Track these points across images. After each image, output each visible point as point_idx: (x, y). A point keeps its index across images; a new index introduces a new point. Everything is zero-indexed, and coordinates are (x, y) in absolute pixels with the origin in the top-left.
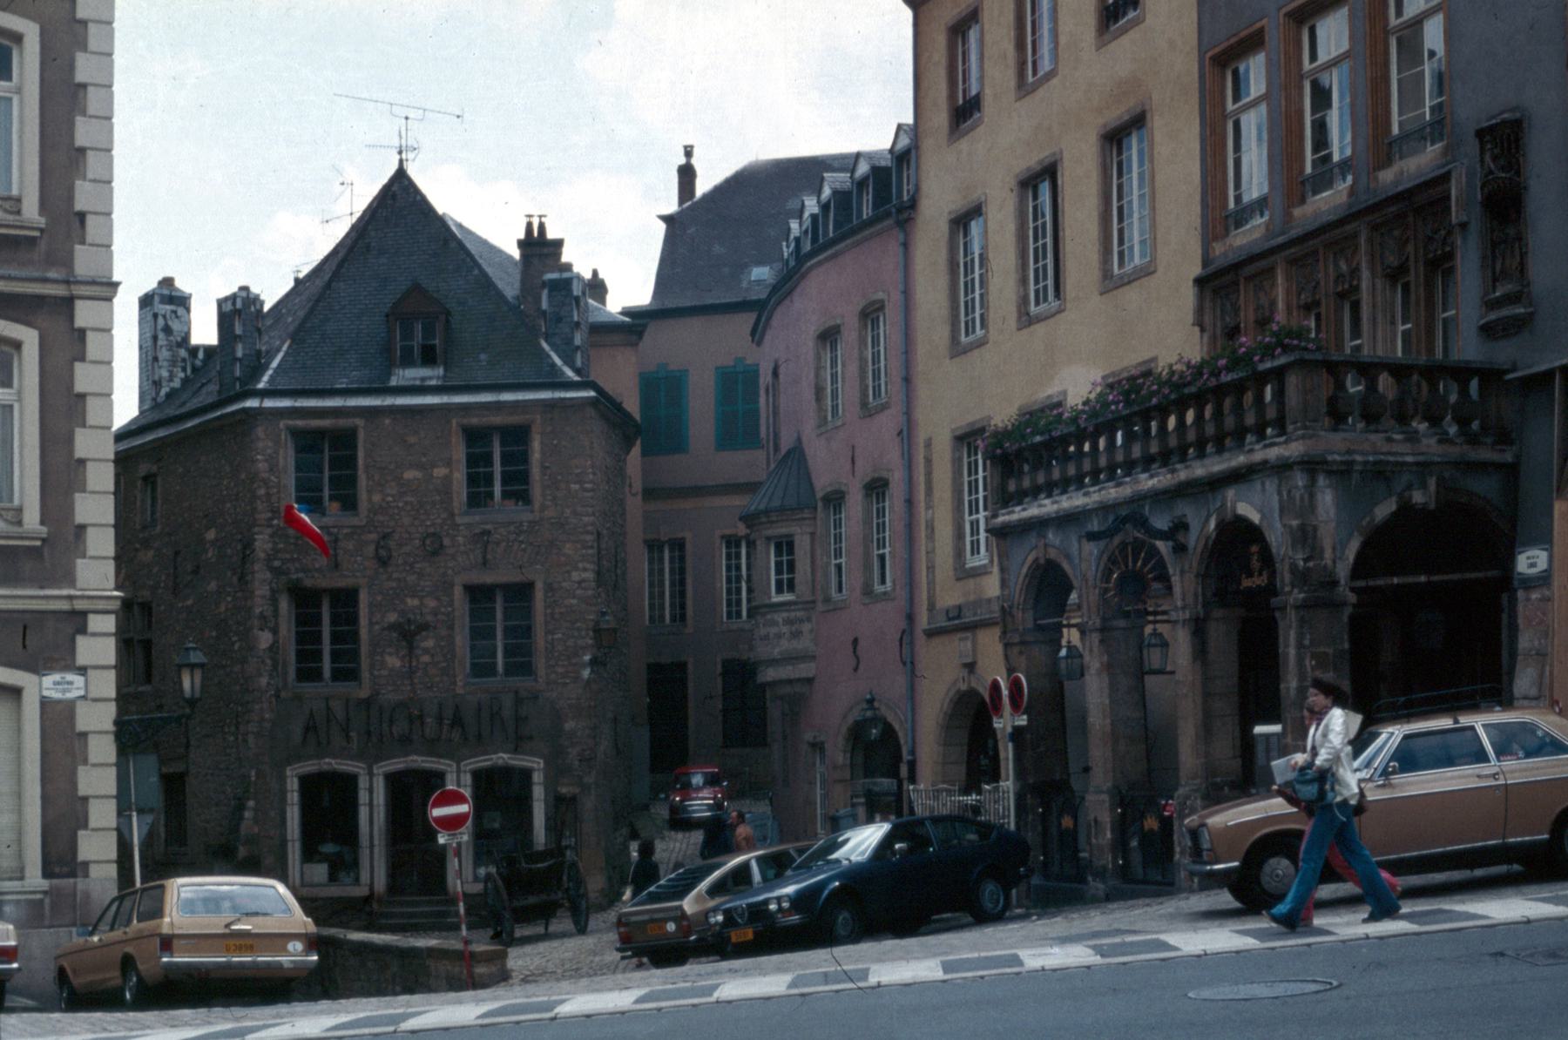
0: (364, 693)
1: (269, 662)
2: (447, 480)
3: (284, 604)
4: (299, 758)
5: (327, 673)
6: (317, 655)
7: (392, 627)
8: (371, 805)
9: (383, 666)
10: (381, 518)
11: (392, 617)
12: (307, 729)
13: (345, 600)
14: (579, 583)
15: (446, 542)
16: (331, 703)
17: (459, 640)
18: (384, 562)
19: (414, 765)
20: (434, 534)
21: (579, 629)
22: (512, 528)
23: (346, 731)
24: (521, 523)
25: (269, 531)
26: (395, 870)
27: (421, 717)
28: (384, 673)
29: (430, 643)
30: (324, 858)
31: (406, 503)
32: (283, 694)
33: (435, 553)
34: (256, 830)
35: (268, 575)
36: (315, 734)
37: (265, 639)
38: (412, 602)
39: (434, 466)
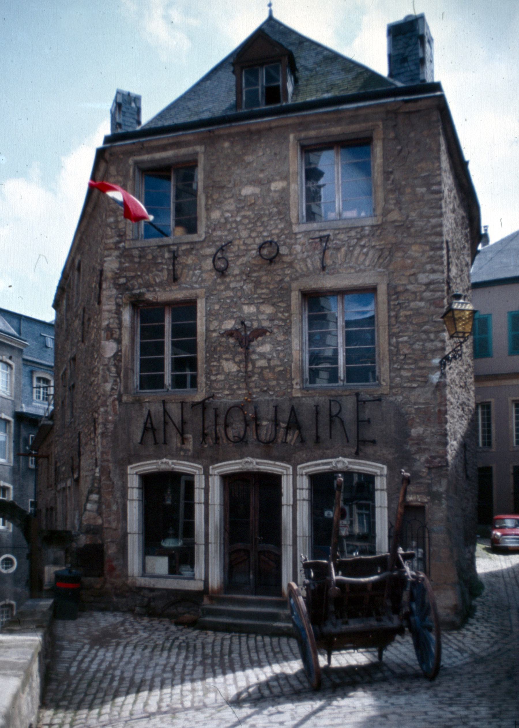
0: (199, 396)
1: (113, 369)
2: (285, 191)
3: (126, 316)
4: (139, 458)
5: (168, 380)
6: (160, 365)
7: (230, 334)
8: (207, 504)
9: (221, 377)
10: (219, 233)
11: (229, 325)
12: (146, 429)
13: (186, 309)
14: (428, 284)
15: (283, 250)
16: (169, 406)
17: (295, 343)
18: (222, 273)
19: (250, 467)
20: (271, 242)
21: (426, 332)
22: (353, 233)
23: (182, 433)
24: (363, 228)
25: (116, 253)
26: (231, 568)
27: (256, 419)
28: (221, 377)
29: (266, 348)
30: (162, 552)
31: (244, 217)
32: (125, 398)
33: (271, 261)
34: (100, 521)
35: (114, 292)
36: (155, 435)
37: (110, 348)
38: (249, 310)
39: (270, 182)
